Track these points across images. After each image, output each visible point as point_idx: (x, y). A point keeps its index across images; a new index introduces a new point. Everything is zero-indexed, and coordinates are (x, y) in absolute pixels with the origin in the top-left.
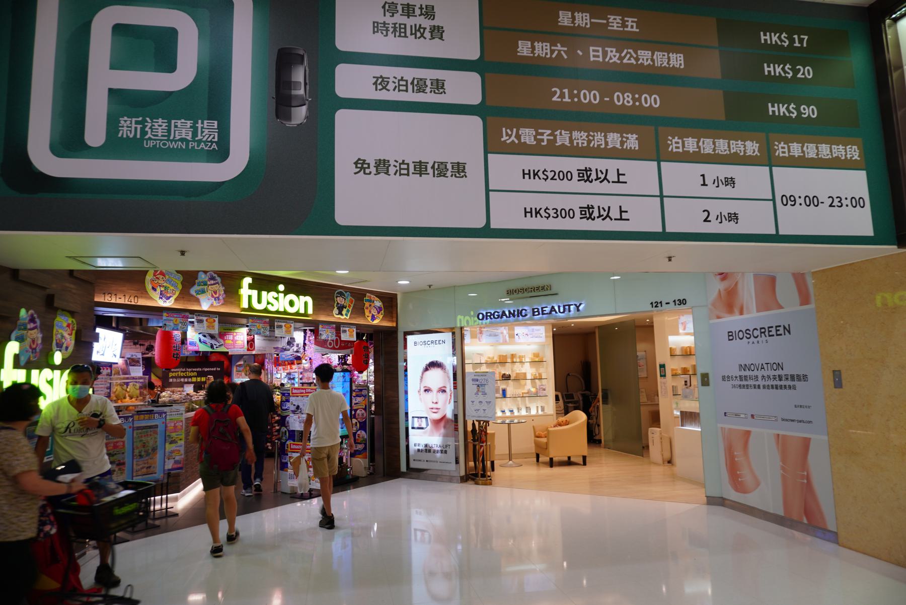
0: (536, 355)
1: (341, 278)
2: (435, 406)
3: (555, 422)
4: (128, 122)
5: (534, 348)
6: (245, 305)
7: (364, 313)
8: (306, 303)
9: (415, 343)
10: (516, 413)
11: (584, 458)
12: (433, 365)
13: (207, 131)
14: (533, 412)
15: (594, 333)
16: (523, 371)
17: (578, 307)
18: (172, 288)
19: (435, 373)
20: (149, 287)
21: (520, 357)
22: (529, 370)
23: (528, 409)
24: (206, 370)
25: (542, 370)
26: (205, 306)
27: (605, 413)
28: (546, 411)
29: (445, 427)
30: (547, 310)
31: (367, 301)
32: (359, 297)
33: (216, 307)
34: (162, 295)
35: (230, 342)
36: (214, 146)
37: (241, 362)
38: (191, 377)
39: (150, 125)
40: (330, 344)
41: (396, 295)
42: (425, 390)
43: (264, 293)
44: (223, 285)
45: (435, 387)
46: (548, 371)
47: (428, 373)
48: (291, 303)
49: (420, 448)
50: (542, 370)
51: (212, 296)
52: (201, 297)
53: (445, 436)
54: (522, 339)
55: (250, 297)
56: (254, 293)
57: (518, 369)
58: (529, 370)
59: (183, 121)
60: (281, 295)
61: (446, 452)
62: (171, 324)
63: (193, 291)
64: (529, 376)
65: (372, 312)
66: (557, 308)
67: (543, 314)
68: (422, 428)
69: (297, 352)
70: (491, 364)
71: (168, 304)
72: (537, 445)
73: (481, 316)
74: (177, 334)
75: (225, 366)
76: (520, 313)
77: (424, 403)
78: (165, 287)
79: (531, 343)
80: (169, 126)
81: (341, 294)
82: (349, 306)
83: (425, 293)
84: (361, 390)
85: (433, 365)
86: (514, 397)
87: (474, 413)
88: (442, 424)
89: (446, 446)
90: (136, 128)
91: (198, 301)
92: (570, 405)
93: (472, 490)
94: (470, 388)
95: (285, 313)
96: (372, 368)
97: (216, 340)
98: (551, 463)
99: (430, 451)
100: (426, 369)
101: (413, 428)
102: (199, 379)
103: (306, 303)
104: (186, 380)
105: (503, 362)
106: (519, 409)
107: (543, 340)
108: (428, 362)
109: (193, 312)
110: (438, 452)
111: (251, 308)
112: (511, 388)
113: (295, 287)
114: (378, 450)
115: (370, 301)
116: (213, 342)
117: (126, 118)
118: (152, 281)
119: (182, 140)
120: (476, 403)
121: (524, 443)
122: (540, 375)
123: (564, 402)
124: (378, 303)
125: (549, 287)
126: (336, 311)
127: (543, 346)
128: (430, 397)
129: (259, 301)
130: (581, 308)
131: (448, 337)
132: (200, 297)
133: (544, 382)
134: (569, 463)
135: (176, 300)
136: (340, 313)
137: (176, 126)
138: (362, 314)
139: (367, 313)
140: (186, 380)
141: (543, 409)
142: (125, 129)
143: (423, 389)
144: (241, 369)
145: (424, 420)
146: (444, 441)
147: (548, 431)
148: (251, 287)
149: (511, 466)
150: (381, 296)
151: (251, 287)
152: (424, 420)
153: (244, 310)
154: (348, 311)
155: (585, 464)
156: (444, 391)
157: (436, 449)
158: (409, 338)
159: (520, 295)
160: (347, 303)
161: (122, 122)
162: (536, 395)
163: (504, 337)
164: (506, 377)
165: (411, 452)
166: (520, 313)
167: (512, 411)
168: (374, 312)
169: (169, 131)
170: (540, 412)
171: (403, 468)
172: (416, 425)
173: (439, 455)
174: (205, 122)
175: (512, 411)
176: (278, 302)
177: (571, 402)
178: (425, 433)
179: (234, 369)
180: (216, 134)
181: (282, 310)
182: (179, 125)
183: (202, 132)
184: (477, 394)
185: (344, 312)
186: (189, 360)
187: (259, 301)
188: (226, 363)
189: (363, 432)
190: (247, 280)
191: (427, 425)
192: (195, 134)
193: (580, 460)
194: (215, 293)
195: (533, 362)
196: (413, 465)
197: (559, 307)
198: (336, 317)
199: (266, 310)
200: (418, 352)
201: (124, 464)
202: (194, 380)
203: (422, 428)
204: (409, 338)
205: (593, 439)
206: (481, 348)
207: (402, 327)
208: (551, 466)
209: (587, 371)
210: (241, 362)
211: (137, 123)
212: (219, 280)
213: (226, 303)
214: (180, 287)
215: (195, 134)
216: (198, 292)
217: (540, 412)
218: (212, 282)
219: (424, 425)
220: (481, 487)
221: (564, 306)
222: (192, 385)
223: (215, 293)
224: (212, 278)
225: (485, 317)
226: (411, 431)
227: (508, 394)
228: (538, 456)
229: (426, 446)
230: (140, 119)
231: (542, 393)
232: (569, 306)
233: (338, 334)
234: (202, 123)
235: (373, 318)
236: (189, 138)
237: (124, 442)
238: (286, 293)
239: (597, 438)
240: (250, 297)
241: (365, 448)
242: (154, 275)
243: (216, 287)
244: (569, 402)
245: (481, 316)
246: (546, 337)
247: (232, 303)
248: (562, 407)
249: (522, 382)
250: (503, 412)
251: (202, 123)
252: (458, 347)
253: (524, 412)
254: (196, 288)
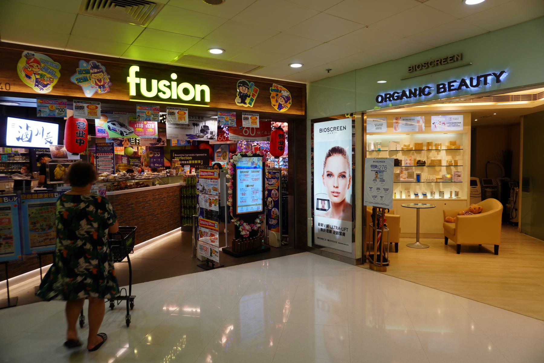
0: (452, 143)
1: (214, 60)
2: (336, 190)
3: (467, 209)
5: (450, 136)
6: (133, 92)
7: (270, 102)
8: (203, 92)
9: (321, 130)
10: (429, 197)
11: (496, 247)
12: (336, 150)
14: (447, 196)
15: (519, 124)
16: (439, 158)
17: (497, 77)
18: (49, 76)
19: (337, 159)
20: (22, 75)
21: (437, 145)
22: (444, 158)
23: (441, 193)
24: (198, 155)
25: (458, 158)
26: (89, 94)
27: (523, 201)
28: (460, 196)
29: (344, 211)
30: (456, 85)
31: (274, 90)
32: (264, 88)
33: (101, 94)
34: (38, 83)
35: (141, 130)
37: (220, 150)
38: (188, 160)
40: (246, 132)
41: (305, 85)
42: (328, 175)
43: (154, 82)
44: (108, 74)
45: (336, 172)
46: (465, 159)
47: (330, 159)
48: (186, 92)
49: (323, 227)
50: (458, 158)
51: (96, 84)
52: (83, 85)
53: (344, 219)
54: (439, 128)
55: (138, 86)
56: (143, 82)
57: (433, 156)
58: (444, 158)
60: (174, 84)
61: (344, 234)
62: (47, 110)
63: (73, 79)
64: (444, 163)
65: (280, 101)
66: (468, 82)
67: (450, 90)
68: (325, 210)
69: (211, 138)
70: (407, 151)
71: (46, 91)
72: (446, 228)
73: (380, 99)
74: (82, 122)
75: (210, 152)
76: (422, 91)
77: (328, 185)
78: (41, 75)
79: (443, 128)
81: (244, 84)
82: (253, 95)
83: (330, 79)
84: (275, 173)
85: (336, 150)
86: (429, 182)
87: (372, 200)
88: (342, 208)
89: (345, 229)
91: (80, 89)
92: (488, 190)
93: (364, 276)
94: (369, 174)
95: (179, 100)
96: (286, 152)
97: (126, 128)
98: (459, 249)
99: (330, 232)
100: (329, 155)
101: (318, 209)
102: (193, 162)
103: (203, 92)
104: (185, 162)
105: (418, 149)
106: (432, 193)
107: (460, 128)
108: (330, 148)
109: (71, 99)
110: (337, 233)
111: (139, 95)
112: (425, 174)
113: (189, 75)
114: (282, 229)
115: (277, 90)
116: (123, 129)
118: (25, 69)
120: (374, 189)
121: (433, 223)
122: (456, 162)
123: (482, 187)
124: (286, 93)
125: (461, 56)
126: (238, 100)
127: (460, 134)
128: (332, 181)
129: (149, 89)
130: (502, 78)
131: (347, 122)
132: (83, 85)
133: (460, 169)
134: (478, 249)
135: (55, 87)
136: (243, 102)
138: (269, 103)
139: (273, 102)
140: (185, 162)
141: (457, 194)
143: (326, 174)
144: (220, 155)
145: (326, 202)
146: (342, 224)
147: (457, 218)
148: (138, 75)
149: (418, 248)
150: (288, 86)
151: (138, 75)
152: (326, 202)
153: (133, 97)
154: (252, 100)
155: (496, 253)
156: (344, 176)
157: (336, 230)
158: (316, 125)
159: (424, 71)
160: (251, 92)
162: (450, 181)
163: (420, 127)
164: (421, 164)
165: (316, 231)
166: (422, 91)
167: (425, 195)
168: (281, 101)
170: (454, 197)
171: (310, 244)
172: (320, 207)
173: (338, 236)
175: (425, 195)
176: (171, 90)
177: (489, 187)
178: (327, 214)
179: (216, 155)
181: (174, 97)
184: (375, 180)
185: (248, 101)
186: (186, 149)
187: (149, 89)
188: (210, 150)
189: (276, 210)
190: (134, 69)
191: (329, 207)
193: (493, 250)
194: (100, 81)
195: (449, 150)
196: (318, 242)
197: (471, 80)
198: (238, 105)
199: (157, 98)
200: (328, 137)
201: (11, 238)
202: (190, 162)
203: (325, 210)
204: (316, 125)
205: (508, 220)
206: (386, 137)
207: (312, 115)
208: (458, 253)
209: (508, 159)
210: (220, 150)
212: (103, 68)
213: (112, 91)
214: (58, 75)
216: (79, 80)
217: (454, 197)
218: (96, 70)
219: (326, 207)
220: (375, 273)
221: (478, 78)
222: (189, 166)
223: (100, 81)
224: (95, 67)
225: (384, 99)
226: (316, 212)
227: (423, 178)
228: (446, 239)
229: (328, 226)
231: (456, 179)
232: (486, 77)
233: (239, 122)
235: (280, 107)
237: (9, 219)
238: (179, 81)
239: (514, 221)
240: (138, 86)
241: (278, 223)
242: (27, 63)
243: (100, 76)
244: (487, 187)
245: (380, 99)
246: (465, 125)
247: (119, 91)
248: (480, 191)
249: (437, 168)
250: (416, 195)
252: (359, 131)
253: (437, 196)
254: (77, 76)
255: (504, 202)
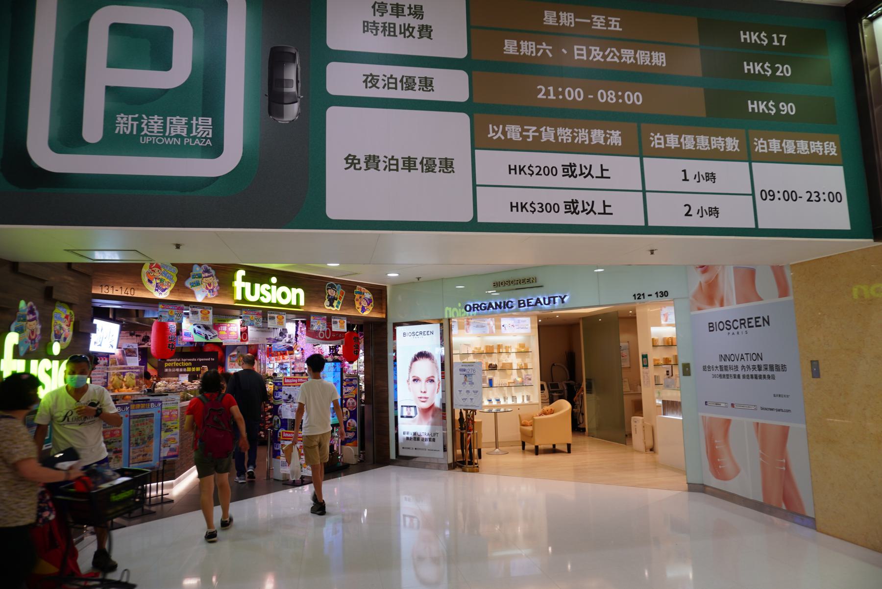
0: (522, 346)
1: (332, 270)
2: (423, 395)
3: (540, 411)
4: (125, 119)
5: (520, 339)
6: (238, 297)
7: (354, 305)
8: (298, 295)
9: (404, 334)
10: (502, 402)
11: (569, 446)
12: (422, 355)
13: (201, 127)
14: (519, 401)
15: (578, 324)
16: (509, 361)
17: (562, 299)
18: (167, 280)
19: (423, 363)
20: (145, 279)
21: (507, 348)
22: (515, 360)
23: (514, 398)
24: (200, 360)
25: (527, 361)
26: (200, 298)
27: (589, 402)
28: (531, 400)
29: (433, 416)
30: (533, 302)
31: (357, 293)
32: (350, 289)
33: (210, 299)
34: (158, 288)
35: (224, 333)
36: (209, 142)
37: (235, 353)
38: (186, 367)
39: (146, 121)
40: (322, 335)
41: (385, 287)
42: (414, 380)
43: (257, 286)
44: (217, 278)
45: (423, 376)
46: (534, 361)
47: (416, 363)
48: (284, 295)
49: (409, 436)
50: (527, 361)
51: (207, 288)
52: (196, 290)
53: (434, 424)
54: (509, 330)
55: (243, 289)
56: (248, 285)
57: (504, 359)
58: (515, 360)
59: (178, 117)
60: (274, 287)
61: (434, 440)
62: (167, 315)
63: (187, 284)
64: (515, 367)
65: (363, 304)
66: (542, 300)
67: (529, 306)
68: (411, 417)
69: (289, 342)
70: (478, 354)
71: (164, 296)
72: (523, 433)
73: (468, 308)
74: (172, 326)
75: (219, 356)
76: (506, 305)
77: (413, 392)
78: (161, 280)
79: (516, 334)
80: (165, 123)
81: (332, 286)
82: (340, 298)
83: (414, 285)
84: (351, 380)
85: (422, 355)
86: (501, 387)
87: (462, 403)
88: (431, 413)
89: (435, 434)
90: (132, 125)
91: (192, 293)
92: (555, 394)
93: (459, 477)
94: (458, 378)
95: (278, 304)
96: (362, 358)
97: (210, 331)
98: (537, 451)
99: (418, 439)
100: (415, 360)
101: (402, 417)
102: (194, 369)
103: (298, 295)
104: (181, 370)
105: (489, 352)
106: (505, 399)
107: (528, 331)
108: (416, 353)
109: (188, 304)
110: (426, 440)
111: (244, 300)
112: (497, 378)
113: (287, 279)
114: (368, 438)
115: (360, 293)
116: (208, 333)
117: (122, 115)
118: (148, 273)
119: (177, 136)
120: (464, 392)
121: (510, 431)
122: (526, 365)
123: (550, 392)
124: (368, 295)
125: (535, 280)
126: (327, 303)
127: (528, 336)
128: (418, 387)
129: (252, 293)
130: (565, 300)
131: (436, 328)
132: (195, 289)
133: (530, 372)
134: (554, 450)
135: (171, 292)
136: (331, 305)
137: (171, 123)
138: (353, 305)
139: (357, 305)
140: (181, 370)
141: (528, 398)
142: (122, 125)
143: (411, 379)
144: (235, 359)
145: (413, 409)
146: (432, 429)
147: (534, 420)
148: (244, 279)
149: (497, 454)
150: (371, 288)
151: (244, 279)
152: (413, 409)
153: (238, 301)
154: (339, 303)
155: (569, 451)
156: (432, 381)
157: (425, 437)
158: (398, 329)
159: (507, 287)
160: (338, 295)
161: (119, 119)
162: (522, 385)
163: (491, 328)
164: (492, 367)
165: (400, 440)
166: (506, 305)
167: (498, 400)
168: (364, 304)
169: (165, 127)
170: (526, 402)
171: (393, 456)
172: (405, 414)
173: (427, 443)
174: (200, 118)
175: (498, 400)
176: (271, 294)
177: (556, 392)
178: (414, 421)
179: (228, 359)
180: (211, 131)
181: (274, 301)
182: (174, 121)
183: (197, 129)
184: (464, 383)
185: (335, 304)
186: (184, 351)
187: (252, 293)
188: (220, 353)
189: (354, 421)
190: (241, 273)
191: (416, 414)
192: (190, 130)
193: (565, 448)
194: (210, 285)
195: (518, 353)
196: (402, 453)
197: (544, 299)
198: (327, 309)
199: (259, 302)
200: (407, 342)
201: (120, 451)
202: (189, 369)
203: (411, 417)
204: (398, 329)
205: (577, 427)
206: (468, 339)
207: (392, 319)
208: (537, 454)
209: (571, 361)
210: (235, 353)
211: (133, 119)
212: (213, 272)
213: (220, 295)
214: (175, 279)
215: (190, 130)
216: (193, 285)
217: (526, 402)
218: (207, 274)
219: (413, 414)
220: (468, 474)
221: (549, 298)
222: (187, 375)
223: (210, 285)
224: (207, 271)
225: (472, 308)
226: (400, 420)
227: (495, 383)
228: (523, 444)
229: (415, 434)
230: (137, 116)
231: (527, 383)
232: (554, 298)
233: (329, 325)
234: (197, 120)
235: (363, 310)
236: (184, 134)
237: (120, 431)
238: (278, 285)
239: (581, 426)
240: (243, 289)
241: (355, 437)
242: (150, 268)
243: (210, 280)
244: (554, 392)
245: (468, 308)
246: (532, 328)
247: (225, 295)
248: (548, 396)
249: (509, 372)
250: (490, 401)
251: (197, 120)
252: (446, 338)
253: (510, 401)
254: (191, 280)
255: (570, 400)
